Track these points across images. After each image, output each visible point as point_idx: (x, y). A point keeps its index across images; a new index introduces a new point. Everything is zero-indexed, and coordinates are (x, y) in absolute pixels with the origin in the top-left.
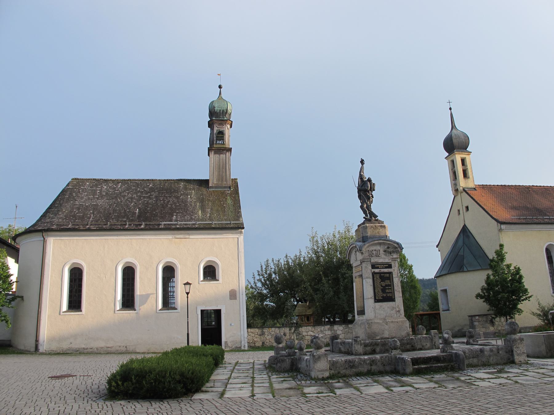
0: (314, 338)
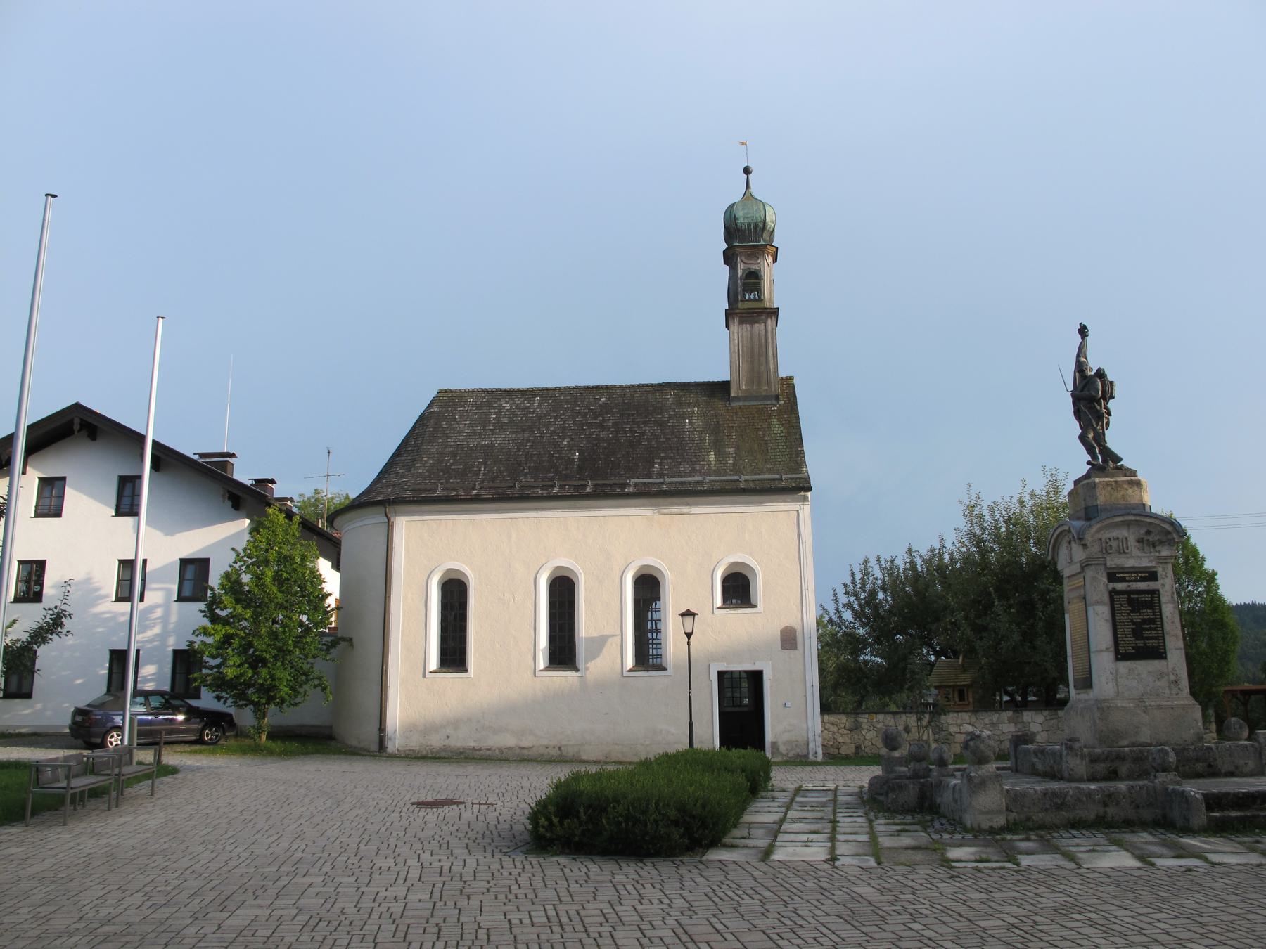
0: (971, 740)
